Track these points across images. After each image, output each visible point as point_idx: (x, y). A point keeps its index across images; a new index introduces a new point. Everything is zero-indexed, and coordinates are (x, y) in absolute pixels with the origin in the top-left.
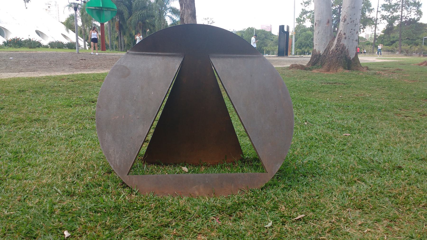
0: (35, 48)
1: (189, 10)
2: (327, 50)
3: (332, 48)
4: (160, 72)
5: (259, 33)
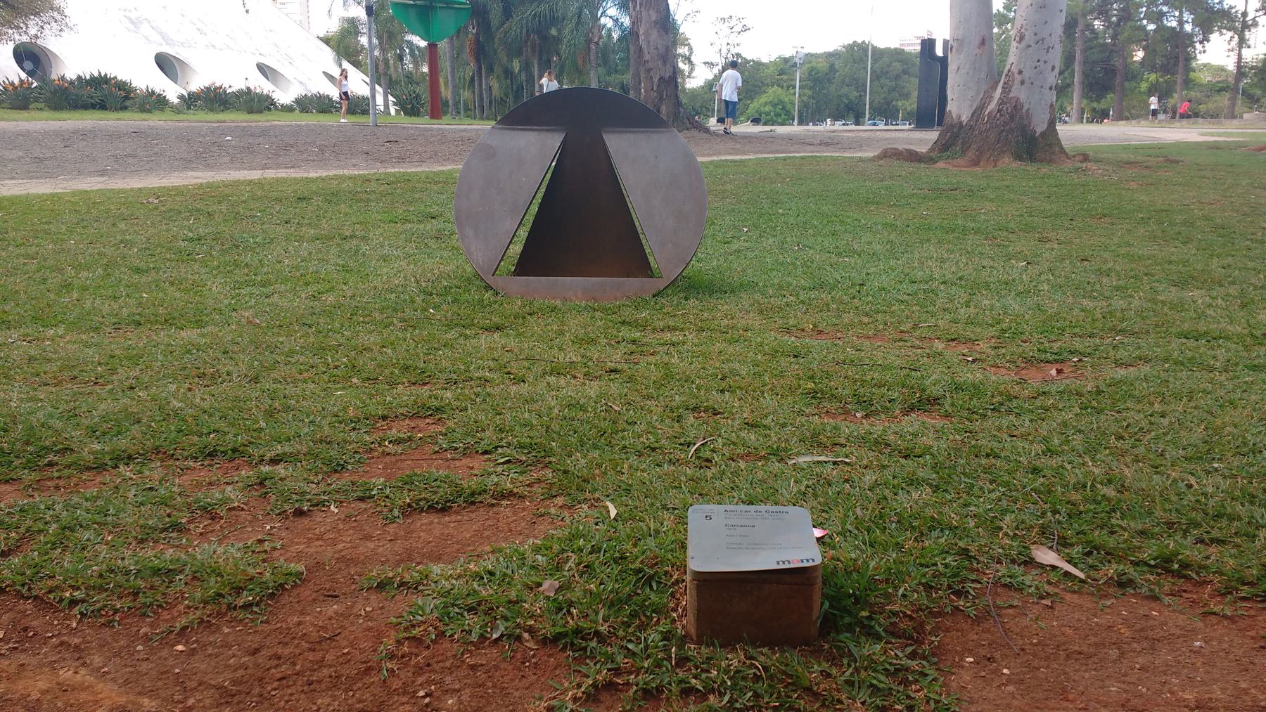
0: (261, 112)
1: (651, 12)
2: (978, 113)
3: (990, 108)
4: (538, 149)
5: (886, 59)
